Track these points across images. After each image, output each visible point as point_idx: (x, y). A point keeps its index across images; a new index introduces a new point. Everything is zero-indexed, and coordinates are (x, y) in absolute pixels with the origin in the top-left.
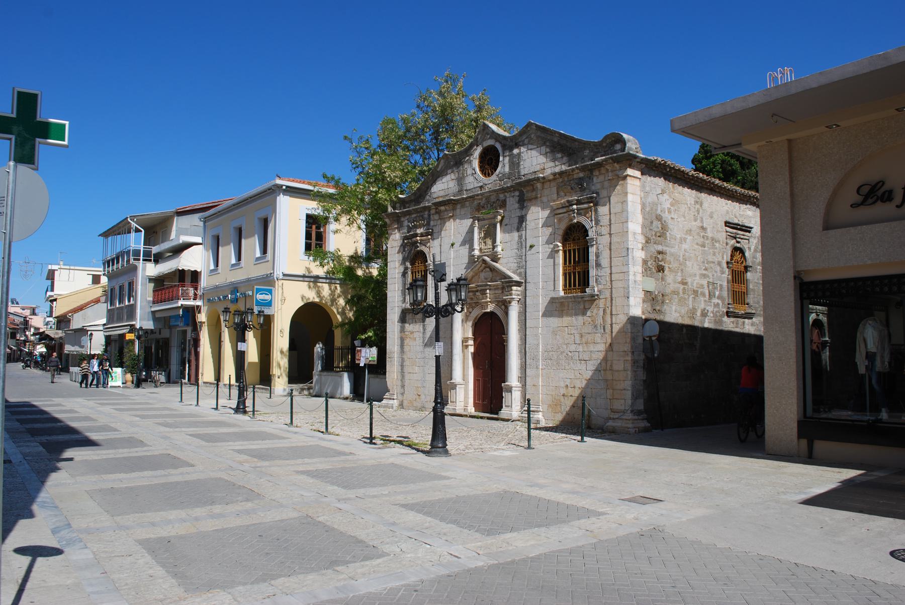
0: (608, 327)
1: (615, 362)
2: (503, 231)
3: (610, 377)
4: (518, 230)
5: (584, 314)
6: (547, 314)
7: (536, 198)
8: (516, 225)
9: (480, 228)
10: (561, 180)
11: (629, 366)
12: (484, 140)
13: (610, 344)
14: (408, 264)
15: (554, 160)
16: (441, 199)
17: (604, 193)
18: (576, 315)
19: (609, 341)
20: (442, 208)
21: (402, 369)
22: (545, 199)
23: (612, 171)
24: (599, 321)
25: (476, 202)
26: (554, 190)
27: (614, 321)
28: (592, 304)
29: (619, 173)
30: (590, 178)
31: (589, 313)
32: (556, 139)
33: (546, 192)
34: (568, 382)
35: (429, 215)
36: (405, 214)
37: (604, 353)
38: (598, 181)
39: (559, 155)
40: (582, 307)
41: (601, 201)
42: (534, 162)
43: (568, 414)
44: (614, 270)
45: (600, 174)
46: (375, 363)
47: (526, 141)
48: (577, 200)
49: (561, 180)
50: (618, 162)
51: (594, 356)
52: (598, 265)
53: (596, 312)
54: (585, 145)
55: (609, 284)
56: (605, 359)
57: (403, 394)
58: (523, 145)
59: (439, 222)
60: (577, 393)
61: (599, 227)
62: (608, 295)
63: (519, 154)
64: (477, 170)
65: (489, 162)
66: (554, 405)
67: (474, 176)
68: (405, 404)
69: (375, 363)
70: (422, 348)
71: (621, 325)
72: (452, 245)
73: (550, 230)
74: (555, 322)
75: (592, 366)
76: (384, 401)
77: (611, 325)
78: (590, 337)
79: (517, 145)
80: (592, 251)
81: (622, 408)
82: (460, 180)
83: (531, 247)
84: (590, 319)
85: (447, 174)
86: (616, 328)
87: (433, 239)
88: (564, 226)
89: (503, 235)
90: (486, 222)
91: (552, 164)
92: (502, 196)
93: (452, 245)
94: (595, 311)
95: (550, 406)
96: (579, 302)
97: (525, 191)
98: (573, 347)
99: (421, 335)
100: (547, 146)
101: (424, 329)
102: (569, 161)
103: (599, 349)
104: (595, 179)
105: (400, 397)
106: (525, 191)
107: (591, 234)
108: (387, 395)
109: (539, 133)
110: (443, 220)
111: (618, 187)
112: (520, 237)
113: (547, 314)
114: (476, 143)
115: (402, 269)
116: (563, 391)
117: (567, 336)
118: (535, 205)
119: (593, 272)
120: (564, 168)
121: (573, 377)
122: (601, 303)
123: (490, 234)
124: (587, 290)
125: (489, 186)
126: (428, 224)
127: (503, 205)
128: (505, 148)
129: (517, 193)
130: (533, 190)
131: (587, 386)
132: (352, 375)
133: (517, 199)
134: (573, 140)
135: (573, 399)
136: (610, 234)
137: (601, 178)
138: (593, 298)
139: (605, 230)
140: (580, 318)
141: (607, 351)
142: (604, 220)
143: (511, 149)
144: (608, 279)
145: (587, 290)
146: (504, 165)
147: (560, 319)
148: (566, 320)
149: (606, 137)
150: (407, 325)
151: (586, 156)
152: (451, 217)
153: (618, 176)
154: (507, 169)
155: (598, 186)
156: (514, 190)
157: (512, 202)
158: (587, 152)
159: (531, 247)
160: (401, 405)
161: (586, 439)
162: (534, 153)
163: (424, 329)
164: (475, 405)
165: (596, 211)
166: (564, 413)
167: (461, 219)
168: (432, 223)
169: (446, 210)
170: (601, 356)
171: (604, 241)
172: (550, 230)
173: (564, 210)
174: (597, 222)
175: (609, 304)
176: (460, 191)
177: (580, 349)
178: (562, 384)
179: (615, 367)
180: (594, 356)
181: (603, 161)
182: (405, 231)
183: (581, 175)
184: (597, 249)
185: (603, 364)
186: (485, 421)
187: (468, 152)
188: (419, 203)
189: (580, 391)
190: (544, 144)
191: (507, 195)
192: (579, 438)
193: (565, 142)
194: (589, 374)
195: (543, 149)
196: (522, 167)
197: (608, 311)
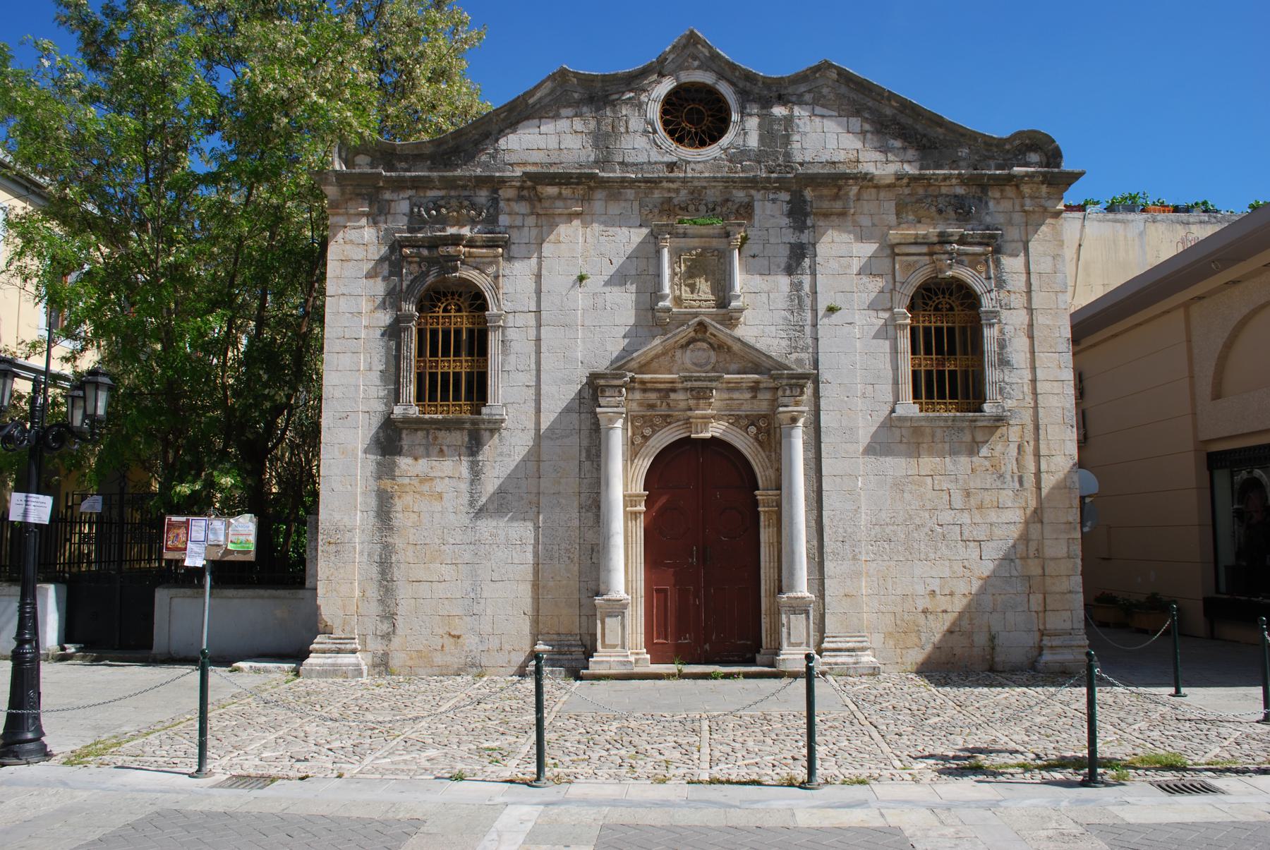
0: (1030, 480)
1: (1047, 542)
2: (748, 270)
3: (1035, 570)
4: (790, 271)
5: (973, 449)
6: (876, 448)
7: (843, 214)
8: (783, 261)
9: (676, 255)
10: (907, 191)
11: (1077, 549)
12: (681, 68)
13: (1035, 511)
14: (410, 308)
15: (884, 150)
16: (539, 169)
17: (1013, 233)
18: (953, 453)
19: (1033, 504)
20: (552, 190)
21: (383, 573)
22: (865, 221)
23: (1032, 197)
24: (1010, 466)
25: (657, 194)
26: (890, 206)
27: (1043, 467)
28: (992, 434)
29: (1049, 204)
30: (982, 201)
31: (984, 451)
32: (888, 111)
33: (867, 206)
34: (935, 585)
35: (495, 201)
36: (399, 185)
37: (1020, 527)
38: (998, 209)
39: (898, 144)
40: (967, 437)
41: (1008, 247)
42: (824, 140)
43: (937, 648)
44: (1040, 374)
45: (1003, 198)
46: (251, 557)
47: (808, 97)
48: (962, 236)
49: (907, 191)
50: (1050, 184)
51: (998, 532)
52: (1004, 363)
53: (1004, 449)
54: (960, 135)
55: (1029, 399)
56: (1025, 538)
57: (387, 637)
58: (800, 103)
59: (531, 220)
60: (958, 605)
61: (1003, 294)
62: (1027, 417)
63: (789, 120)
64: (659, 126)
65: (695, 116)
66: (901, 632)
67: (642, 140)
68: (397, 660)
69: (251, 557)
70: (466, 520)
71: (1060, 475)
72: (581, 278)
73: (879, 283)
74: (896, 466)
75: (994, 551)
76: (313, 660)
77: (1038, 474)
78: (987, 497)
79: (782, 100)
80: (990, 334)
81: (1068, 625)
82: (603, 140)
83: (831, 310)
84: (987, 463)
85: (557, 117)
86: (1048, 482)
87: (510, 259)
88: (918, 279)
89: (745, 276)
90: (696, 242)
91: (878, 156)
92: (740, 195)
93: (581, 278)
94: (999, 448)
95: (889, 635)
96: (961, 429)
97: (814, 198)
98: (947, 516)
99: (464, 486)
100: (866, 120)
101: (476, 473)
102: (922, 159)
103: (1009, 519)
104: (991, 204)
105: (377, 646)
106: (814, 198)
107: (987, 304)
108: (320, 641)
109: (843, 90)
110: (547, 220)
111: (1043, 228)
112: (797, 287)
113: (876, 448)
114: (659, 69)
115: (385, 318)
116: (922, 604)
117: (930, 494)
118: (839, 228)
119: (992, 375)
120: (910, 169)
121: (947, 573)
122: (1014, 434)
123: (710, 267)
124: (484, 410)
125: (699, 167)
126: (492, 220)
127: (746, 211)
128: (745, 97)
129: (785, 196)
130: (836, 197)
131: (983, 590)
132: (64, 588)
133: (786, 207)
134: (937, 121)
135: (948, 620)
136: (1030, 310)
137: (1006, 205)
138: (1000, 420)
139: (1018, 300)
140: (964, 460)
141: (1027, 523)
142: (1016, 282)
143: (766, 104)
144: (1027, 389)
145: (484, 410)
146: (745, 132)
147: (913, 461)
148: (928, 463)
149: (1019, 134)
150: (404, 462)
151: (961, 159)
152: (578, 215)
153: (1045, 209)
154: (753, 141)
155: (1000, 219)
156: (779, 189)
157: (770, 213)
158: (963, 152)
159: (831, 310)
160: (382, 665)
161: (1183, 690)
162: (831, 126)
163: (476, 473)
164: (650, 645)
165: (998, 263)
166: (929, 648)
167: (605, 224)
168: (504, 220)
169: (560, 196)
170: (1015, 532)
171: (1014, 320)
172: (879, 283)
173: (924, 249)
174: (1001, 284)
175: (1029, 435)
176: (604, 162)
177: (965, 518)
178: (920, 589)
179: (1049, 552)
180: (998, 532)
181: (1027, 175)
182: (402, 223)
183: (960, 191)
184: (1001, 332)
185: (1021, 548)
186: (741, 682)
187: (635, 80)
188: (448, 165)
189: (965, 601)
190: (857, 113)
191: (758, 195)
192: (1172, 690)
193: (910, 121)
194: (987, 568)
195: (856, 123)
196: (796, 146)
197: (1029, 449)
